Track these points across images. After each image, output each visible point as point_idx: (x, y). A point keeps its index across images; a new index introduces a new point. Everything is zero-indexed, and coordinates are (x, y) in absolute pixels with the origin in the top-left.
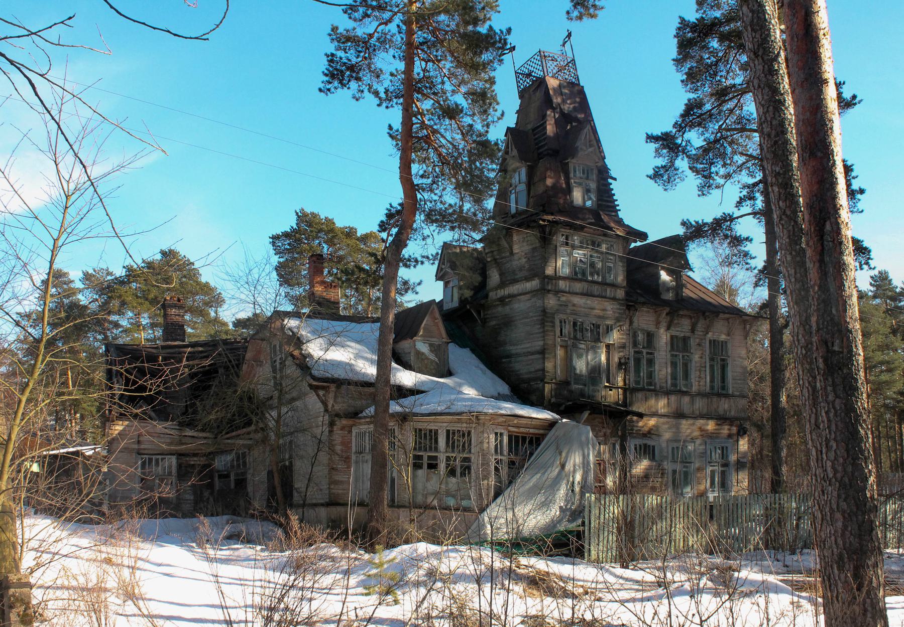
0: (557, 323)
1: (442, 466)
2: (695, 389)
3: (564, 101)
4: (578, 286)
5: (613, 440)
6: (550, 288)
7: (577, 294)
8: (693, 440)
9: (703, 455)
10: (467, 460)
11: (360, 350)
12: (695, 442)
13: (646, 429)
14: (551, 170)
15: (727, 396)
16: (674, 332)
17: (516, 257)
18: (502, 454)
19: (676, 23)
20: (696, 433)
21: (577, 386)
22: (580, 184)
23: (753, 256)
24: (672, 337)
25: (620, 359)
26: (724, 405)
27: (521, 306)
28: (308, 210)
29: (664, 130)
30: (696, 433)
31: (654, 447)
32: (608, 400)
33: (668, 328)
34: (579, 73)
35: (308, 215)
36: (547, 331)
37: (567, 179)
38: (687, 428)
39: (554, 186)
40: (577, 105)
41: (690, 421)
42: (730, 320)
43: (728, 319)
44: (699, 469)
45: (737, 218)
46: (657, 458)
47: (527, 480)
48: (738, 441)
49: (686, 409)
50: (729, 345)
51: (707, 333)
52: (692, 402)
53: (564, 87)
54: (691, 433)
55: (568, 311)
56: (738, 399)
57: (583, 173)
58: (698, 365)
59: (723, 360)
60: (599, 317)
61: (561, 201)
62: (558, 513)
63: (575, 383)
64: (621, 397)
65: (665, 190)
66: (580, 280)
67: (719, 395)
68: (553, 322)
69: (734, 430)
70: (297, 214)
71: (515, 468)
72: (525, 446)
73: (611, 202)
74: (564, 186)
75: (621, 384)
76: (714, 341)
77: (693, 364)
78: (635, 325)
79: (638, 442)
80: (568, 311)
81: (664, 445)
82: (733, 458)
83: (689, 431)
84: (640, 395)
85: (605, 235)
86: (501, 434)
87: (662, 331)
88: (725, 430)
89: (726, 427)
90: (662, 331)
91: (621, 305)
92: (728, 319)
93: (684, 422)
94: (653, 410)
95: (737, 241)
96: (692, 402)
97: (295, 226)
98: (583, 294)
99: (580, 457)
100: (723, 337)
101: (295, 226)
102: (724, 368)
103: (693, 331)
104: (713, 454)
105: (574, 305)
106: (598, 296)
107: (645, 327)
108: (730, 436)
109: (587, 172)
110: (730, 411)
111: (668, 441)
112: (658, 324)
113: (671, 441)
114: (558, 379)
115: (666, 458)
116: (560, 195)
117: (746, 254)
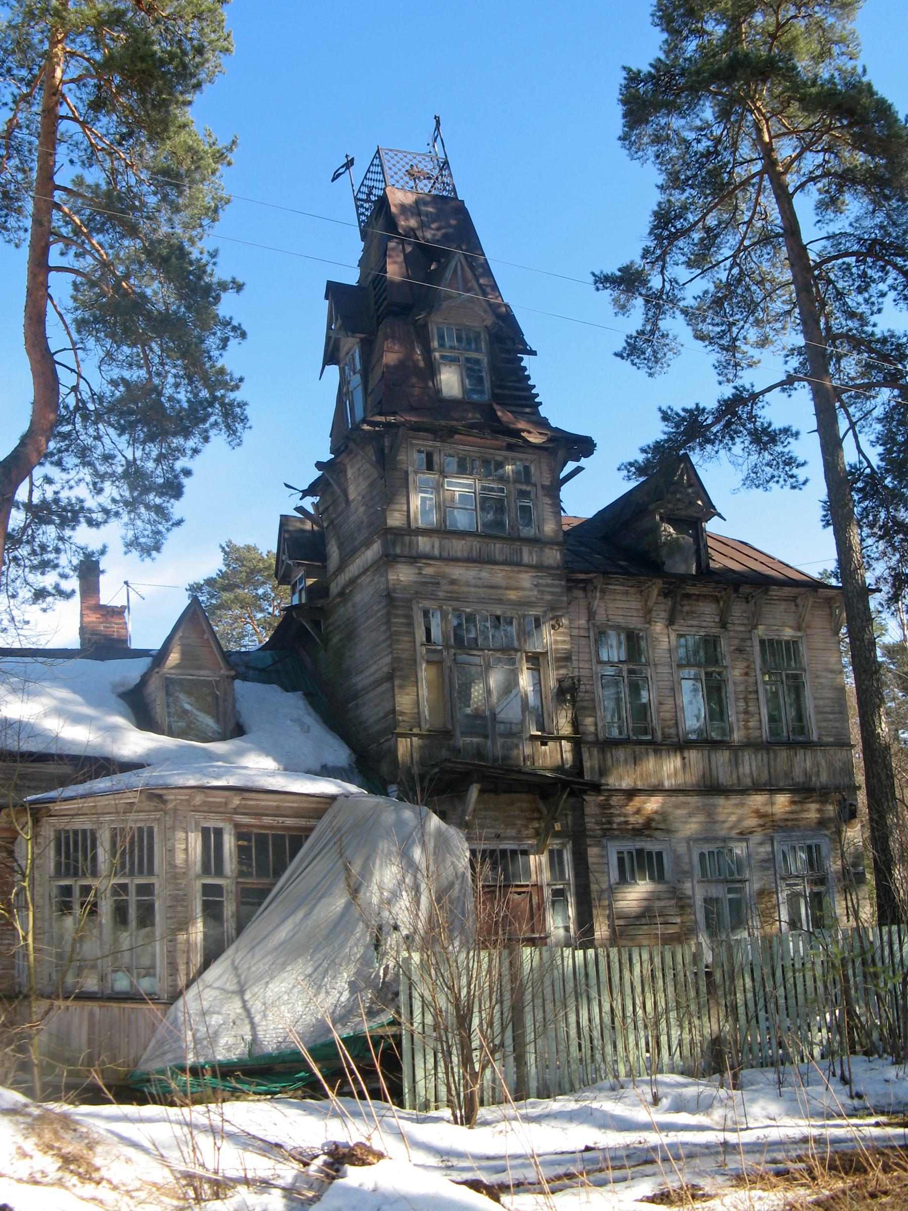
0: (419, 619)
1: (106, 907)
2: (737, 736)
3: (423, 225)
5: (554, 843)
6: (398, 550)
7: (456, 560)
8: (744, 836)
9: (769, 862)
10: (146, 889)
11: (63, 701)
12: (747, 840)
13: (638, 820)
14: (393, 337)
15: (808, 745)
17: (353, 505)
18: (219, 872)
19: (620, 78)
20: (752, 822)
22: (453, 360)
23: (801, 460)
25: (560, 681)
26: (803, 764)
27: (364, 596)
28: (240, 542)
29: (624, 262)
30: (752, 822)
31: (660, 854)
32: (540, 763)
33: (671, 622)
35: (238, 549)
36: (397, 633)
37: (427, 351)
38: (734, 813)
39: (401, 365)
40: (451, 230)
41: (735, 800)
42: (799, 601)
43: (794, 599)
44: (761, 893)
45: (763, 393)
46: (667, 876)
47: (277, 926)
48: (839, 832)
49: (724, 776)
50: (803, 649)
51: (755, 627)
52: (736, 762)
53: (426, 204)
54: (740, 820)
55: (441, 594)
56: (832, 751)
57: (459, 339)
58: (741, 688)
59: (796, 677)
61: (416, 391)
62: (346, 995)
63: (464, 734)
64: (568, 756)
65: (651, 375)
67: (791, 745)
68: (409, 617)
69: (831, 810)
70: (223, 548)
71: (253, 899)
72: (270, 853)
73: (523, 390)
74: (422, 364)
75: (566, 729)
76: (771, 641)
77: (731, 688)
78: (601, 617)
80: (441, 594)
81: (682, 849)
82: (834, 866)
83: (733, 818)
84: (621, 753)
85: (510, 447)
86: (219, 833)
87: (659, 627)
88: (812, 812)
89: (814, 806)
92: (794, 599)
93: (721, 801)
94: (654, 781)
95: (765, 438)
96: (736, 762)
97: (224, 569)
99: (409, 871)
100: (788, 633)
101: (224, 569)
102: (797, 688)
103: (723, 625)
104: (790, 860)
105: (453, 582)
107: (621, 621)
108: (822, 823)
109: (467, 339)
110: (818, 774)
111: (689, 840)
112: (647, 616)
113: (697, 840)
114: (426, 726)
115: (689, 874)
116: (414, 380)
117: (790, 461)
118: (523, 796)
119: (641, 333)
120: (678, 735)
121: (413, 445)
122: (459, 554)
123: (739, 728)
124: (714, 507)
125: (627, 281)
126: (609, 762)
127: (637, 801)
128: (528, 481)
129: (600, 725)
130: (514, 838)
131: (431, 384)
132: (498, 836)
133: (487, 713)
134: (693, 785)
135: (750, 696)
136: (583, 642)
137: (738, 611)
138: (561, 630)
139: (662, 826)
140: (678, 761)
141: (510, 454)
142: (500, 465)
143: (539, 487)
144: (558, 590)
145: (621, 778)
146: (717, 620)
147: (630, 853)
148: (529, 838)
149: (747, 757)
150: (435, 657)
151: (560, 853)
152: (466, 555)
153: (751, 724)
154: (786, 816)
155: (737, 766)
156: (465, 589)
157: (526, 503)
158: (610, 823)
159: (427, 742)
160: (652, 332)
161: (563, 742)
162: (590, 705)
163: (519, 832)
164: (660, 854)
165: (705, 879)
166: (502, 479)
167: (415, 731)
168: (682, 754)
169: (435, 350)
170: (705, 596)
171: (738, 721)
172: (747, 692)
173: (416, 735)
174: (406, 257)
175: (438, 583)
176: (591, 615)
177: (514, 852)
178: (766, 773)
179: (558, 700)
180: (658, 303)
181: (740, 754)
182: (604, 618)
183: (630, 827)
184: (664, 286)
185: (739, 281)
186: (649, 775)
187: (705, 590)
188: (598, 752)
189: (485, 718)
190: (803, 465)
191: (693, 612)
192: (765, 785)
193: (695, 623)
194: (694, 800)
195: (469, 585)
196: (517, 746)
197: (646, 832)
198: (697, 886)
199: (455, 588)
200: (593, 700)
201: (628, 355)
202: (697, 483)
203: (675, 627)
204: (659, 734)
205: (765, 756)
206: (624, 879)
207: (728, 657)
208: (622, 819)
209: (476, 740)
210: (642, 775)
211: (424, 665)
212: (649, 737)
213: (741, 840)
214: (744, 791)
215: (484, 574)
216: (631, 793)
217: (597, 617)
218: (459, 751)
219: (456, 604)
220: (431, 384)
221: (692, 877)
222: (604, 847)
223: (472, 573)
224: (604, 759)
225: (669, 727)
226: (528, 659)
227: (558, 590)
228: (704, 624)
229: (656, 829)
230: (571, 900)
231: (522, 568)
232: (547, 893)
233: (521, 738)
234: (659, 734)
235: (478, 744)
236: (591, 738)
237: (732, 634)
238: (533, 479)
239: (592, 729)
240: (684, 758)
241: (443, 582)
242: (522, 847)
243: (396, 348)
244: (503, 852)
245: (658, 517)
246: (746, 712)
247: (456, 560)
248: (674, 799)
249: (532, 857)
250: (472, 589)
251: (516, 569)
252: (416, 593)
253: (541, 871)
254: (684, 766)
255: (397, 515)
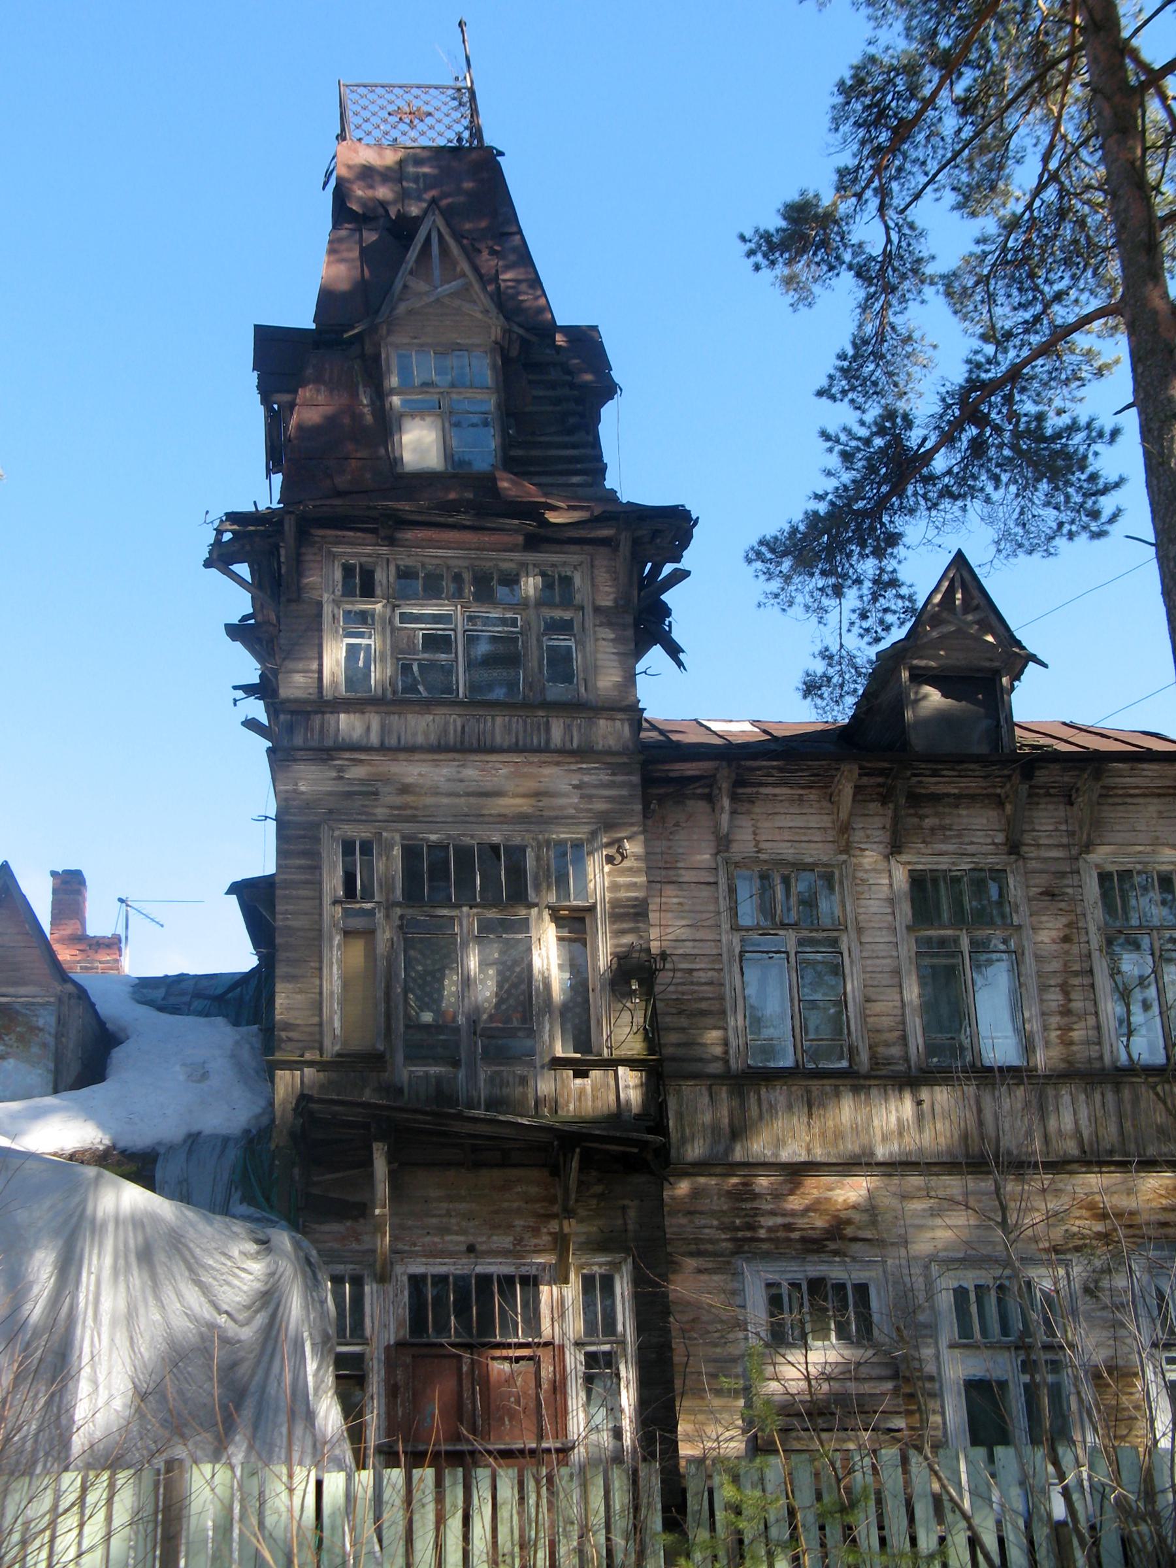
4: (419, 726)
7: (412, 749)
16: (921, 857)
21: (420, 1070)
24: (918, 881)
31: (862, 1290)
34: (483, 121)
37: (380, 394)
55: (381, 812)
58: (1056, 965)
60: (522, 819)
63: (410, 1059)
66: (426, 705)
74: (369, 419)
79: (786, 1272)
80: (381, 812)
84: (778, 1095)
87: (870, 858)
90: (870, 858)
91: (615, 769)
94: (851, 1146)
98: (440, 749)
103: (1014, 848)
105: (405, 789)
106: (509, 750)
114: (332, 1048)
118: (535, 1173)
119: (859, 343)
120: (907, 1059)
121: (335, 556)
122: (420, 740)
123: (1047, 1044)
124: (1018, 643)
125: (803, 236)
126: (754, 1112)
127: (814, 1188)
128: (567, 601)
129: (733, 1043)
130: (505, 1253)
131: (382, 451)
132: (471, 1249)
133: (461, 1020)
134: (939, 1154)
135: (1076, 981)
136: (705, 892)
137: (1047, 823)
138: (627, 863)
139: (868, 1235)
140: (907, 1108)
141: (530, 557)
142: (511, 581)
143: (589, 610)
144: (624, 792)
145: (779, 1143)
146: (1000, 838)
147: (795, 1285)
148: (538, 1251)
149: (1066, 1099)
150: (357, 923)
151: (608, 1284)
152: (433, 739)
153: (1076, 1035)
154: (1163, 1217)
155: (1043, 1118)
156: (429, 800)
157: (562, 641)
158: (752, 1227)
159: (334, 1076)
160: (881, 337)
161: (621, 1070)
162: (715, 1006)
163: (519, 1241)
164: (862, 1290)
165: (965, 1340)
166: (524, 604)
167: (308, 1056)
168: (914, 1095)
169: (393, 392)
170: (973, 798)
171: (1046, 1028)
172: (1067, 971)
173: (311, 1064)
174: (363, 251)
175: (376, 793)
176: (723, 843)
177: (507, 1282)
178: (1113, 1129)
179: (613, 991)
180: (886, 277)
181: (1050, 1092)
182: (750, 849)
183: (796, 1235)
184: (889, 241)
185: (1062, 213)
186: (839, 1135)
187: (972, 785)
188: (731, 1094)
189: (457, 1029)
190: (1117, 485)
191: (943, 828)
192: (1111, 1152)
193: (950, 848)
194: (952, 1185)
195: (437, 794)
196: (523, 1081)
197: (832, 1246)
198: (945, 1353)
199: (409, 799)
200: (722, 998)
201: (844, 393)
202: (983, 602)
203: (904, 858)
204: (864, 1057)
205: (1110, 1097)
206: (779, 1339)
207: (1024, 909)
208: (780, 1220)
209: (433, 1070)
210: (823, 1134)
211: (337, 939)
212: (844, 1064)
213: (1050, 1264)
214: (1058, 1166)
215: (470, 772)
216: (797, 1172)
217: (735, 847)
218: (400, 1091)
219: (409, 828)
220: (382, 451)
221: (935, 1337)
222: (737, 1274)
223: (445, 771)
224: (742, 1106)
225: (887, 1044)
226: (557, 919)
227: (624, 792)
228: (971, 849)
229: (855, 1239)
230: (628, 1373)
231: (545, 757)
232: (574, 1361)
233: (532, 1064)
234: (864, 1057)
235: (439, 1079)
236: (716, 1068)
237: (1033, 865)
238: (578, 598)
239: (718, 1051)
240: (919, 1103)
241: (384, 790)
242: (524, 1270)
243: (321, 398)
244: (485, 1281)
245: (905, 675)
246: (1066, 1012)
247: (412, 749)
248: (896, 1180)
249: (544, 1290)
250: (446, 801)
251: (535, 758)
252: (331, 811)
253: (562, 1315)
254: (920, 1117)
255: (299, 679)
